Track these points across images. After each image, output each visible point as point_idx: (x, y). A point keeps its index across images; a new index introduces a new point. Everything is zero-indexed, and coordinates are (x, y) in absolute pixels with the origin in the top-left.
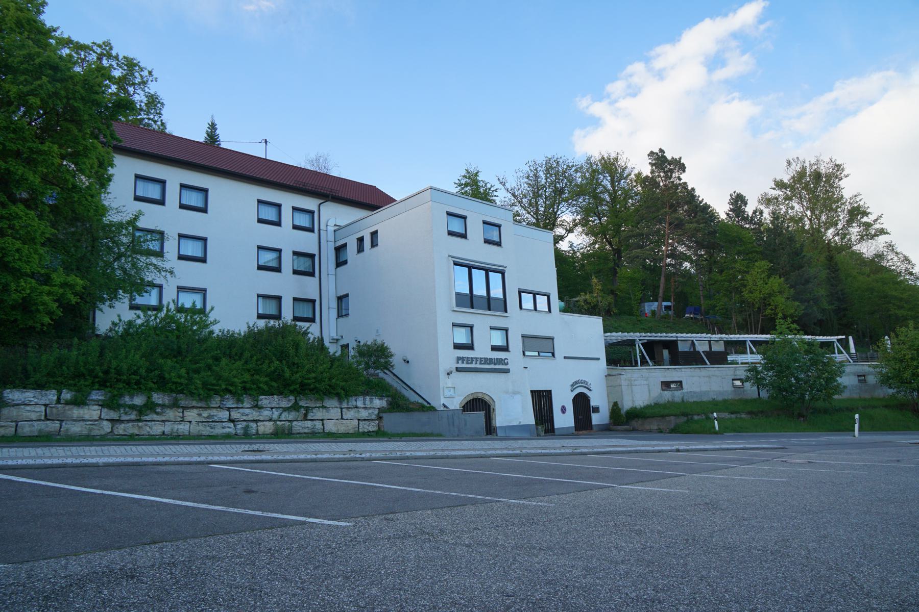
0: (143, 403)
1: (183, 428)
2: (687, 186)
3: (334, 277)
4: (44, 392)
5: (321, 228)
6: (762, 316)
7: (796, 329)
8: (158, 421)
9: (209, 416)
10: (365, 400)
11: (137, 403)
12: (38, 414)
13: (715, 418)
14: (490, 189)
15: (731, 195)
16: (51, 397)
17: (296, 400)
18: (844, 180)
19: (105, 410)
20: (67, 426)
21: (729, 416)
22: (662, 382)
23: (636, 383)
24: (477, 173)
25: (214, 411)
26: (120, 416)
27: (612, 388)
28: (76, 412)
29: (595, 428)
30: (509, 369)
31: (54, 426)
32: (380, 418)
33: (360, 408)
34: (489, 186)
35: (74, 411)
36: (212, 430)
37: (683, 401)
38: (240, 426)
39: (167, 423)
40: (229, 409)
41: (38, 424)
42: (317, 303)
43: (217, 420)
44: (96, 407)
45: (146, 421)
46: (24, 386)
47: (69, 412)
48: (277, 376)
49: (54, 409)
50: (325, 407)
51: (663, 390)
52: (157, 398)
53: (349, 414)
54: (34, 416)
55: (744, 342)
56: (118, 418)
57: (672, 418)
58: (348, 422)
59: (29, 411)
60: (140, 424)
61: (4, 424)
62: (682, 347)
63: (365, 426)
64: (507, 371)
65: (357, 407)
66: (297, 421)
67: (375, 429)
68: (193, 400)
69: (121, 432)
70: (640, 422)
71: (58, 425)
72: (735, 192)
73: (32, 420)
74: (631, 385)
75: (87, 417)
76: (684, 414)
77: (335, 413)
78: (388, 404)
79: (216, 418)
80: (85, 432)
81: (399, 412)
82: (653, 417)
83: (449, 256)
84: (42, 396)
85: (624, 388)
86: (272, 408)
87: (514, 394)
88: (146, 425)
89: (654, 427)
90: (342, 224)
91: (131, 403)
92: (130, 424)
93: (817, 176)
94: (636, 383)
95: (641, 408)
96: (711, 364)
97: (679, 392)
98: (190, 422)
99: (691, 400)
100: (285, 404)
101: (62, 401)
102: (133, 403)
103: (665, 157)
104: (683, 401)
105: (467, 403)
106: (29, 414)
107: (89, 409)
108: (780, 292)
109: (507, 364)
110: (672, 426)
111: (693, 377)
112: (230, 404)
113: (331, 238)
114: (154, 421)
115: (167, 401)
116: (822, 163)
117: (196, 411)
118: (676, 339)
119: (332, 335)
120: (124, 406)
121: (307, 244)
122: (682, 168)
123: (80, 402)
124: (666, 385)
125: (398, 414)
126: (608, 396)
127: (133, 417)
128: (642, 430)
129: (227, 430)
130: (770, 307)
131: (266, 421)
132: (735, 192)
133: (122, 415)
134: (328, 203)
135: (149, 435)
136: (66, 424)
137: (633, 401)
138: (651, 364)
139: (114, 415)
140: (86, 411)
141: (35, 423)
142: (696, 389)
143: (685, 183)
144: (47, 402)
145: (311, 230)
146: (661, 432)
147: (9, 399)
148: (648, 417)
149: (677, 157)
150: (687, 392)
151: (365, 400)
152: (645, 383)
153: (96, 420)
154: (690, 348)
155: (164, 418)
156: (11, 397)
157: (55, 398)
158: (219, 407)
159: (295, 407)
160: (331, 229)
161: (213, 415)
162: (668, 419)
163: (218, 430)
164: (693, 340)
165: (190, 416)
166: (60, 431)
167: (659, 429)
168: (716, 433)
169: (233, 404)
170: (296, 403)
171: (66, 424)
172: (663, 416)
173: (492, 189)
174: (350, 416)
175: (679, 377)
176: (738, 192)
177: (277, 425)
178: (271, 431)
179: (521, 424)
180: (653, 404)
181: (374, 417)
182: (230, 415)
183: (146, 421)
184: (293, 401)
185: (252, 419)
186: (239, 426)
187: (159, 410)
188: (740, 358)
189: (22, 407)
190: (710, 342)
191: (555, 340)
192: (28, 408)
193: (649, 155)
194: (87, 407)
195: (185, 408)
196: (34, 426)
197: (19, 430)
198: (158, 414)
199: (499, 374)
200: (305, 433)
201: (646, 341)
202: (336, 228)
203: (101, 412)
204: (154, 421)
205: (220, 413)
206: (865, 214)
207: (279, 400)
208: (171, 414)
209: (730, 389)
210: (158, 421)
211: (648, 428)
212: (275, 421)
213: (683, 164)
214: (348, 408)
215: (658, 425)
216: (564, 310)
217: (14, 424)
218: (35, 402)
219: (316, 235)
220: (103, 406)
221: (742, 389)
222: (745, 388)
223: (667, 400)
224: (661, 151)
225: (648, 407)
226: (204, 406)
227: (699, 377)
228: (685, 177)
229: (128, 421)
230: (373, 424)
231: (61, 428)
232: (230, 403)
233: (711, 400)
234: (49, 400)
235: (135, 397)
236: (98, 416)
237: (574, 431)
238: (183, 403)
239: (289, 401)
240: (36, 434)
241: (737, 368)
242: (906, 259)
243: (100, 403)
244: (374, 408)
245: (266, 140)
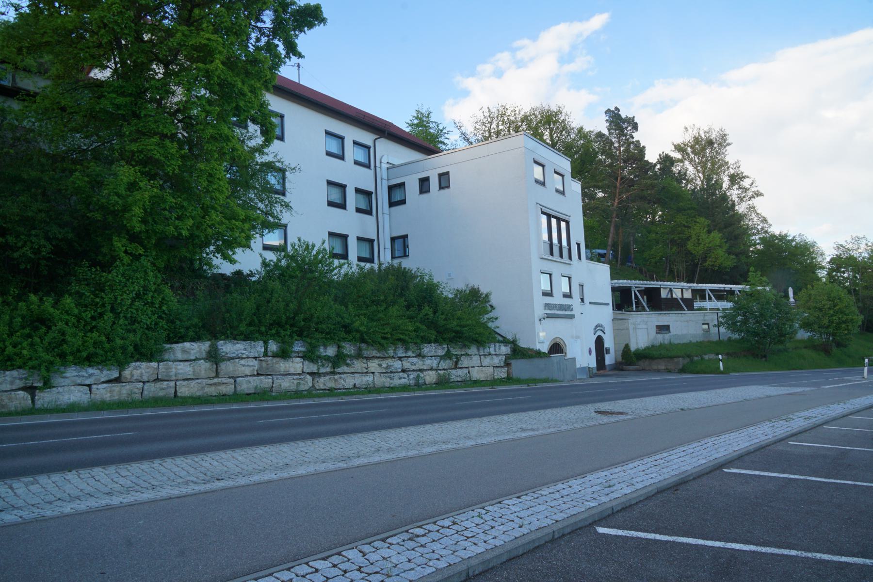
0: (334, 353)
4: (253, 343)
7: (765, 282)
8: (349, 373)
9: (388, 367)
12: (252, 368)
13: (721, 360)
14: (442, 131)
15: (660, 155)
17: (448, 347)
18: (727, 148)
19: (306, 362)
20: (278, 381)
21: (715, 357)
26: (319, 369)
27: (617, 332)
29: (608, 368)
32: (507, 365)
33: (493, 355)
34: (441, 127)
36: (392, 381)
37: (670, 343)
38: (413, 375)
40: (400, 358)
41: (254, 380)
42: (376, 243)
43: (394, 371)
44: (298, 360)
45: (339, 373)
46: (236, 336)
47: (277, 366)
48: (432, 324)
49: (263, 363)
50: (468, 355)
52: (349, 349)
53: (487, 361)
54: (248, 371)
55: (704, 290)
56: (316, 371)
59: (244, 365)
60: (336, 377)
61: (225, 381)
62: (664, 294)
63: (498, 373)
64: (572, 317)
65: (490, 354)
67: (505, 376)
68: (373, 350)
69: (322, 387)
71: (270, 381)
72: (663, 153)
73: (247, 376)
74: (636, 329)
75: (292, 371)
76: (689, 356)
77: (475, 360)
78: (511, 351)
81: (522, 358)
82: (661, 357)
83: (537, 204)
85: (631, 332)
86: (431, 357)
88: (341, 378)
91: (325, 354)
92: (328, 377)
93: (710, 143)
95: (643, 350)
96: (688, 310)
97: (668, 335)
98: (373, 373)
99: (676, 342)
100: (441, 352)
101: (270, 354)
102: (327, 354)
103: (620, 115)
104: (670, 343)
106: (244, 368)
107: (293, 362)
108: (720, 247)
109: (572, 310)
110: (681, 367)
112: (401, 353)
113: (385, 176)
114: (345, 373)
116: (713, 131)
118: (659, 287)
119: (564, 290)
120: (319, 357)
121: (364, 179)
122: (635, 127)
123: (284, 354)
124: (663, 329)
127: (328, 370)
128: (650, 370)
130: (710, 259)
132: (663, 153)
136: (277, 379)
137: (637, 343)
138: (648, 310)
139: (313, 368)
140: (291, 364)
141: (251, 379)
143: (638, 141)
145: (368, 167)
146: (670, 372)
147: (223, 352)
153: (299, 374)
154: (667, 295)
155: (353, 370)
156: (224, 350)
157: (263, 350)
159: (448, 355)
160: (385, 166)
161: (391, 366)
163: (397, 382)
164: (670, 288)
165: (372, 367)
167: (667, 369)
168: (722, 373)
170: (448, 351)
171: (277, 379)
172: (671, 358)
173: (444, 131)
178: (434, 380)
179: (582, 366)
182: (33, 401)
183: (339, 373)
185: (418, 368)
186: (411, 377)
188: (707, 304)
189: (237, 360)
190: (682, 289)
191: (584, 287)
192: (243, 362)
193: (606, 113)
194: (291, 360)
195: (368, 359)
196: (250, 382)
197: (238, 388)
198: (348, 365)
200: (458, 381)
201: (643, 288)
208: (358, 365)
209: (701, 332)
210: (349, 373)
211: (655, 367)
212: (436, 370)
214: (485, 355)
216: (590, 258)
217: (232, 380)
218: (247, 355)
219: (371, 172)
220: (304, 357)
224: (617, 109)
225: (647, 348)
226: (382, 356)
228: (637, 136)
229: (326, 374)
230: (503, 370)
231: (273, 383)
232: (401, 352)
233: (689, 342)
235: (328, 348)
236: (301, 370)
239: (443, 348)
240: (252, 391)
242: (765, 220)
245: (299, 64)
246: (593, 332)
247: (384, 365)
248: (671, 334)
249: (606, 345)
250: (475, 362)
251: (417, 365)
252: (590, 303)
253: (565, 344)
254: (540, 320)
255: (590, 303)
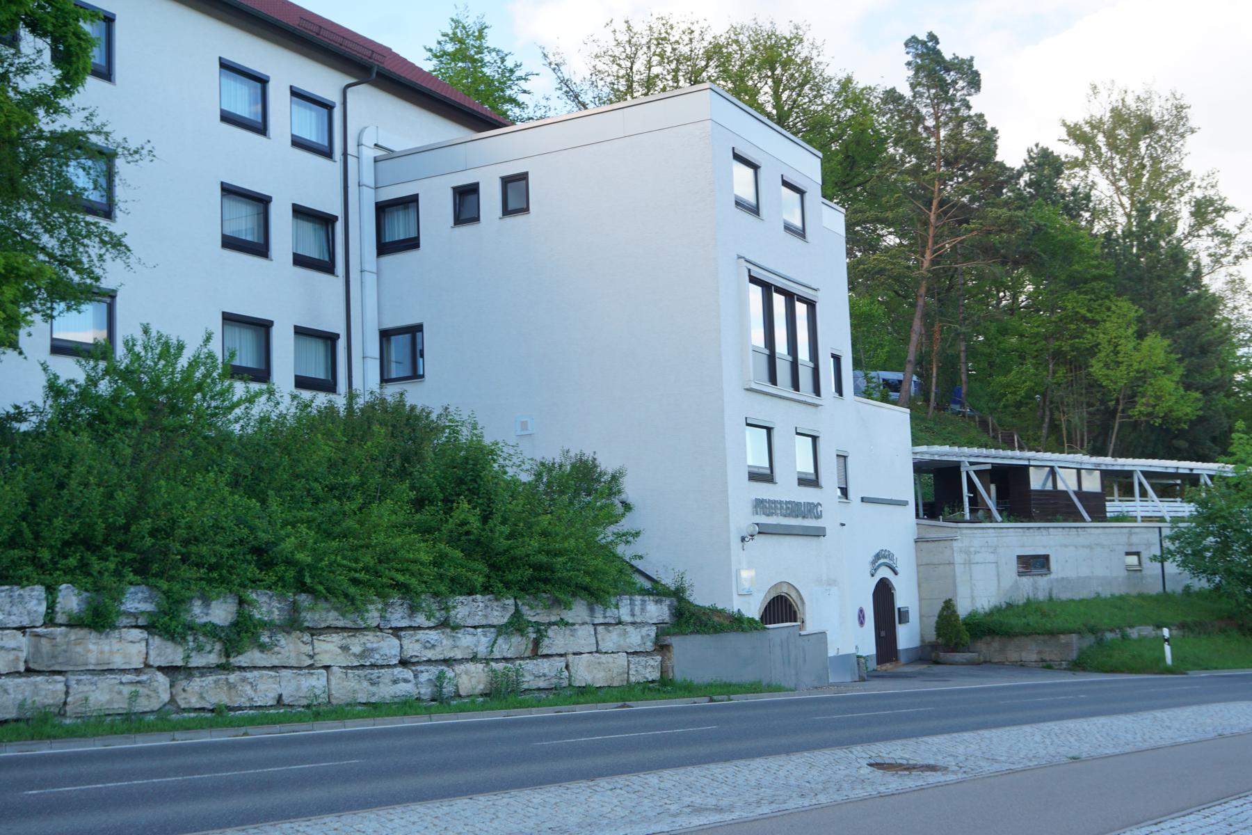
1: (297, 687)
2: (985, 122)
3: (375, 276)
4: (17, 591)
5: (350, 151)
6: (1122, 417)
8: (265, 668)
9: (366, 653)
10: (632, 603)
11: (216, 621)
12: (11, 656)
13: (1167, 640)
14: (512, 71)
15: (1029, 151)
16: (32, 605)
17: (516, 605)
19: (156, 641)
20: (81, 688)
22: (1019, 557)
23: (978, 558)
24: (481, 31)
25: (370, 636)
28: (95, 648)
30: (824, 529)
31: (47, 691)
32: (661, 648)
33: (627, 624)
34: (510, 63)
35: (91, 647)
36: (374, 689)
37: (1051, 599)
39: (284, 672)
40: (396, 632)
42: (341, 344)
43: (380, 662)
44: (136, 634)
45: (241, 668)
47: (79, 649)
49: (44, 641)
50: (567, 624)
51: (1020, 574)
52: (267, 606)
53: (611, 639)
56: (180, 663)
57: (1074, 637)
58: (608, 658)
60: (233, 677)
62: (1037, 481)
64: (819, 533)
65: (620, 623)
66: (523, 659)
67: (655, 675)
69: (195, 702)
70: (996, 644)
75: (118, 662)
79: (377, 656)
80: (121, 705)
82: (1029, 633)
83: (740, 257)
84: (12, 603)
85: (959, 570)
87: (829, 585)
88: (244, 680)
89: (1031, 656)
90: (398, 145)
91: (205, 620)
93: (1148, 126)
94: (978, 558)
97: (1046, 578)
98: (327, 668)
100: (499, 616)
101: (60, 618)
103: (938, 53)
104: (1051, 599)
105: (769, 603)
107: (121, 639)
108: (1167, 370)
111: (1066, 546)
113: (368, 178)
114: (255, 668)
115: (277, 612)
117: (336, 639)
118: (1026, 463)
122: (974, 82)
124: (1034, 564)
125: (699, 637)
126: (919, 586)
127: (213, 659)
129: (402, 688)
131: (467, 660)
132: (1037, 145)
133: (193, 654)
134: (364, 88)
135: (251, 708)
137: (973, 598)
138: (999, 519)
139: (173, 654)
140: (116, 646)
142: (1071, 574)
143: (981, 116)
144: (26, 622)
145: (327, 153)
146: (1049, 667)
148: (1016, 635)
149: (964, 55)
150: (1057, 580)
151: (632, 603)
152: (991, 558)
153: (137, 671)
154: (1044, 484)
155: (275, 661)
157: (43, 608)
158: (378, 627)
159: (516, 625)
160: (369, 154)
161: (372, 650)
162: (1063, 639)
163: (387, 691)
165: (326, 652)
166: (65, 703)
167: (1043, 661)
169: (403, 618)
170: (517, 614)
172: (1053, 634)
174: (611, 645)
175: (1045, 547)
176: (1043, 144)
177: (493, 671)
178: (481, 687)
179: (840, 654)
180: (1004, 606)
181: (649, 646)
183: (241, 668)
184: (512, 610)
185: (441, 657)
186: (424, 677)
187: (265, 639)
195: (314, 631)
198: (263, 648)
199: (775, 538)
200: (539, 689)
201: (989, 467)
202: (380, 153)
203: (147, 645)
204: (255, 668)
205: (382, 644)
206: (1222, 210)
207: (486, 607)
208: (290, 648)
210: (265, 668)
211: (1013, 656)
212: (487, 661)
213: (977, 74)
215: (1040, 652)
216: (865, 393)
219: (334, 167)
220: (150, 628)
221: (1139, 574)
222: (1144, 572)
223: (1026, 596)
224: (933, 37)
225: (997, 610)
226: (350, 624)
227: (1076, 547)
228: (978, 104)
230: (652, 663)
232: (397, 615)
233: (1093, 595)
234: (29, 613)
237: (873, 665)
238: (309, 618)
239: (504, 607)
241: (1133, 530)
243: (141, 622)
244: (647, 624)
246: (868, 568)
247: (356, 649)
248: (1052, 576)
249: (900, 603)
250: (583, 642)
251: (438, 649)
252: (863, 500)
253: (802, 599)
254: (743, 539)
255: (863, 500)
